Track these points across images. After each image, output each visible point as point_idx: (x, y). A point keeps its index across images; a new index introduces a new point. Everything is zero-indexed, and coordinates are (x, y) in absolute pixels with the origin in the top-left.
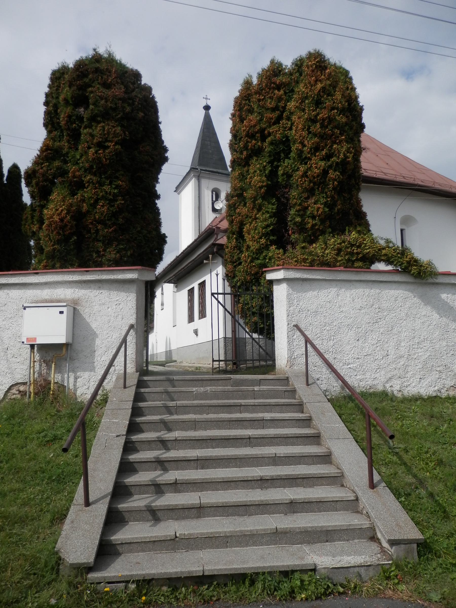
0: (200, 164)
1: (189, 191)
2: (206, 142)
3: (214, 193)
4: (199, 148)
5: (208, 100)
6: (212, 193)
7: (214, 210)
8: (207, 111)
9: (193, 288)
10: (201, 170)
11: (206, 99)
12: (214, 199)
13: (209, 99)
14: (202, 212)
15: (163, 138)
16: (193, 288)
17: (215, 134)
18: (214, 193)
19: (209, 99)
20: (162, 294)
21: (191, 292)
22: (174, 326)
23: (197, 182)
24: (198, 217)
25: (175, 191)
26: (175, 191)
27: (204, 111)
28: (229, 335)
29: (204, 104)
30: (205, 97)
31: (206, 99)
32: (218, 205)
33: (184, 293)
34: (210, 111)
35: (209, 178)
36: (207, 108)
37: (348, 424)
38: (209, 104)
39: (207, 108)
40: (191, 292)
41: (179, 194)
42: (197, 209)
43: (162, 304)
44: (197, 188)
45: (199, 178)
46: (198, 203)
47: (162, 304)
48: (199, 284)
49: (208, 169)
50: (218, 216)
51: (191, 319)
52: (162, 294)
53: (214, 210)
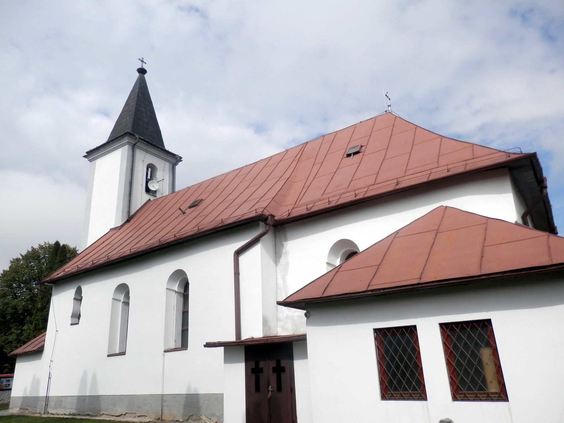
2: (141, 108)
3: (150, 169)
6: (147, 169)
7: (148, 190)
10: (140, 139)
11: (142, 61)
12: (149, 177)
15: (555, 225)
22: (109, 356)
23: (131, 150)
25: (85, 157)
26: (85, 157)
27: (137, 74)
29: (140, 67)
31: (142, 61)
34: (146, 76)
35: (147, 151)
37: (374, 119)
38: (145, 67)
39: (142, 71)
42: (128, 185)
44: (131, 158)
50: (152, 198)
53: (148, 190)
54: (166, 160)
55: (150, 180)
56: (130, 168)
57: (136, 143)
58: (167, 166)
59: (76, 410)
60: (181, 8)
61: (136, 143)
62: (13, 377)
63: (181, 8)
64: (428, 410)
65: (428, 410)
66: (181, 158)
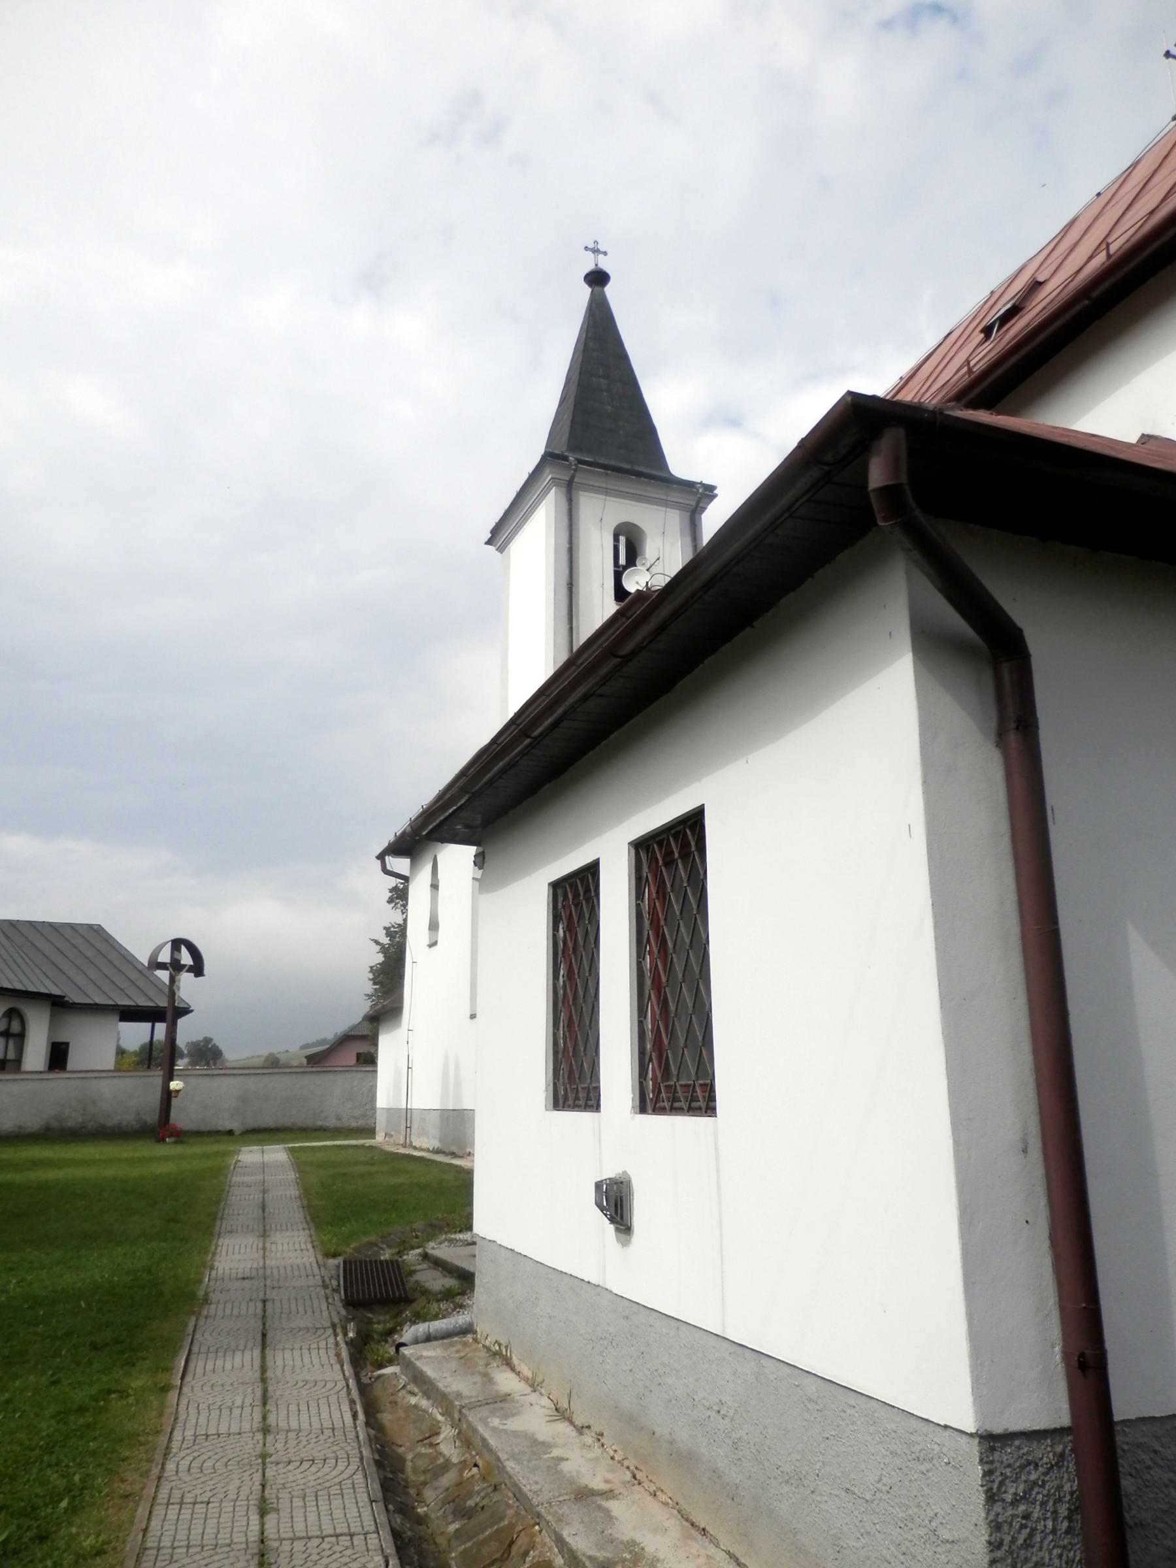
0: (574, 446)
1: (539, 532)
2: (594, 379)
3: (622, 539)
4: (571, 400)
5: (601, 256)
8: (597, 289)
9: (593, 869)
10: (580, 462)
11: (596, 251)
12: (622, 561)
13: (605, 253)
14: (581, 602)
16: (593, 869)
17: (623, 357)
18: (622, 539)
19: (605, 253)
20: (435, 886)
21: (575, 897)
24: (565, 620)
25: (487, 543)
26: (487, 543)
27: (587, 291)
28: (1044, 1404)
29: (590, 267)
30: (591, 246)
31: (596, 251)
32: (637, 578)
33: (527, 906)
34: (609, 290)
35: (606, 492)
36: (597, 279)
38: (605, 264)
39: (597, 279)
40: (575, 897)
41: (501, 549)
42: (564, 592)
43: (434, 926)
44: (565, 521)
45: (570, 490)
46: (567, 571)
47: (434, 926)
48: (643, 846)
49: (602, 461)
51: (574, 1085)
52: (435, 886)
54: (666, 504)
55: (625, 568)
56: (565, 545)
57: (573, 477)
58: (674, 519)
59: (440, 1141)
60: (887, 25)
61: (573, 477)
62: (376, 1071)
63: (887, 25)
64: (718, 1171)
65: (718, 1171)
66: (711, 488)
